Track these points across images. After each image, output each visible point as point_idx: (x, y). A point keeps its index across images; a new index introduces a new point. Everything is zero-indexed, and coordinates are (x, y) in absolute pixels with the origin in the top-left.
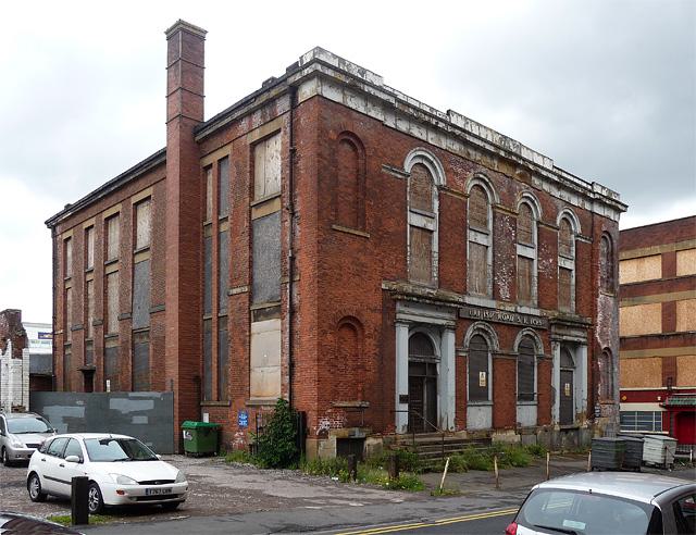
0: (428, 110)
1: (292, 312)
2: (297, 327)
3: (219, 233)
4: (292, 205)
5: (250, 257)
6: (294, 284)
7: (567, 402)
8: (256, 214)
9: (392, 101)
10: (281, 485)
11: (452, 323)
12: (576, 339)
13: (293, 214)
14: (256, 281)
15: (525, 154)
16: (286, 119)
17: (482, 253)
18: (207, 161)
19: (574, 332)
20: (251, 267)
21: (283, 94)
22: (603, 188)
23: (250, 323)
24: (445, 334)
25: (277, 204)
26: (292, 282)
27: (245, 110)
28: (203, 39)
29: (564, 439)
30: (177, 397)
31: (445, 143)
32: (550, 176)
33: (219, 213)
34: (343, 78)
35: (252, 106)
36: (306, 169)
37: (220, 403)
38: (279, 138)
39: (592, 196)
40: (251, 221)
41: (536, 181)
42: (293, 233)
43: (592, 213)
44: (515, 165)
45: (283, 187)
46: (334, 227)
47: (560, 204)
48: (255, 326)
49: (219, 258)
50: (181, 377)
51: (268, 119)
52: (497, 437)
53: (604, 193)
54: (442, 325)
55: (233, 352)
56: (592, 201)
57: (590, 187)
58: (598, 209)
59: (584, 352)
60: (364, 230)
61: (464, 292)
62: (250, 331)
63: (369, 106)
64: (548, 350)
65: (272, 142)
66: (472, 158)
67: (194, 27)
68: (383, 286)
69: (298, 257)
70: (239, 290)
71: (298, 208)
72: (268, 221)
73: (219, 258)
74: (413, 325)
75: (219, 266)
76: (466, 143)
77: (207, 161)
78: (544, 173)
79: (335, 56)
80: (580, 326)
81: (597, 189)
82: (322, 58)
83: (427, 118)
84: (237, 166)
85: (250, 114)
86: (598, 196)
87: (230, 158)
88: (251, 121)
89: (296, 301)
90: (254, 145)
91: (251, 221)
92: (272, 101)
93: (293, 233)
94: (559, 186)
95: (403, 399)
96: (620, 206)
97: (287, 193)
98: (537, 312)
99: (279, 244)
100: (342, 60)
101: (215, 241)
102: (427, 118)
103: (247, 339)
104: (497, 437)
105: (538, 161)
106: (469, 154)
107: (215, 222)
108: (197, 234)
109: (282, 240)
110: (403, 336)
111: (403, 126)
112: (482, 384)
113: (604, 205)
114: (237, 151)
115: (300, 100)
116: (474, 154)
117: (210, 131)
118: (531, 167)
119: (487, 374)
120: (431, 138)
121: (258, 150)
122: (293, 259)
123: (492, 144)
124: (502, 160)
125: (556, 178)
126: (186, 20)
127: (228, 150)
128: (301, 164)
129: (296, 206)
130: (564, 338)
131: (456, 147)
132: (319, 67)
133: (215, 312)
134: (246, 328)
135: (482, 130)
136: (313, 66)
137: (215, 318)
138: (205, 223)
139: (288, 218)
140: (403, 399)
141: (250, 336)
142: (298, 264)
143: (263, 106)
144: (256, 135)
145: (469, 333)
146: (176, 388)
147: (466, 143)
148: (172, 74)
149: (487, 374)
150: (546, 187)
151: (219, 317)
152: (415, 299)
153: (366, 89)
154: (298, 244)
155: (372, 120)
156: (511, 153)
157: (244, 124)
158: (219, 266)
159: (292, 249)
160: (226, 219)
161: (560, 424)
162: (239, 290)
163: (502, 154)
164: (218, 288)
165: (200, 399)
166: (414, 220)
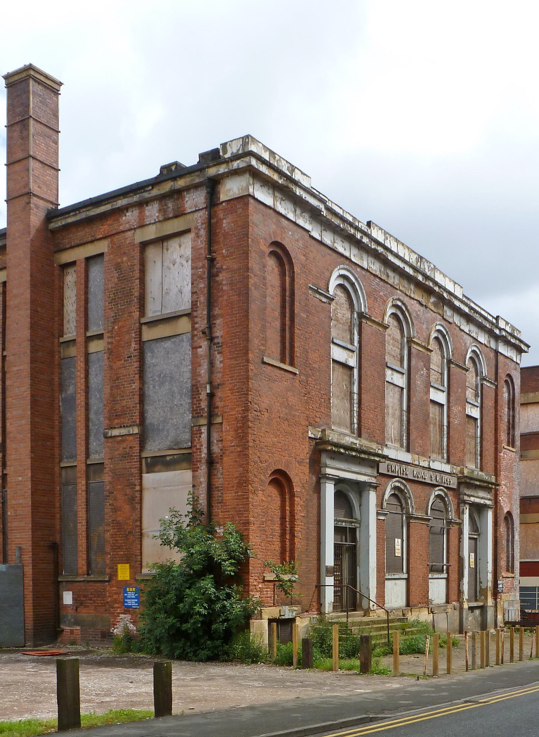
0: (350, 219)
1: (211, 462)
2: (219, 480)
3: (87, 355)
4: (210, 326)
5: (141, 389)
6: (214, 429)
7: (475, 572)
8: (148, 334)
9: (322, 207)
10: (487, 671)
11: (374, 480)
12: (482, 501)
13: (211, 339)
14: (148, 422)
15: (439, 278)
16: (201, 217)
17: (397, 396)
18: (66, 257)
19: (481, 494)
20: (142, 401)
21: (196, 187)
22: (507, 323)
23: (141, 473)
24: (364, 495)
25: (184, 325)
26: (210, 425)
27: (136, 198)
28: (56, 93)
29: (470, 619)
30: (29, 570)
31: (366, 262)
32: (463, 307)
33: (86, 328)
34: (275, 177)
35: (146, 195)
36: (231, 284)
37: (92, 577)
38: (187, 241)
39: (497, 332)
40: (141, 344)
41: (448, 313)
42: (211, 364)
43: (497, 352)
44: (429, 292)
45: (194, 304)
46: (266, 359)
47: (469, 340)
48: (149, 478)
49: (87, 386)
50: (35, 545)
51: (171, 215)
52: (412, 617)
53: (508, 329)
54: (365, 483)
55: (115, 510)
56: (497, 338)
57: (494, 321)
58: (502, 349)
59: (490, 514)
60: (292, 364)
61: (383, 444)
62: (141, 485)
63: (298, 211)
64: (459, 513)
65: (173, 244)
66: (391, 281)
67: (46, 77)
68: (310, 435)
69: (219, 394)
70: (123, 431)
71: (218, 333)
72: (168, 344)
73: (87, 386)
74: (339, 481)
75: (87, 398)
76: (386, 263)
77: (66, 257)
78: (457, 303)
79: (266, 148)
80: (486, 486)
81: (502, 325)
82: (253, 148)
83: (352, 231)
84: (118, 267)
85: (142, 204)
86: (504, 333)
87: (106, 258)
88: (141, 213)
89: (216, 449)
90: (144, 245)
91: (141, 344)
92: (177, 194)
93: (211, 364)
94: (469, 319)
95: (330, 571)
96: (523, 346)
97: (202, 312)
98: (447, 468)
99: (188, 375)
100: (272, 153)
101: (81, 365)
102: (352, 231)
103: (138, 495)
104: (412, 617)
105: (450, 287)
106: (388, 276)
107: (81, 340)
108: (52, 353)
109: (194, 373)
110: (329, 490)
111: (328, 238)
112: (398, 554)
113: (508, 343)
114: (117, 249)
115: (223, 197)
116: (394, 279)
117: (78, 218)
118: (445, 295)
119: (402, 541)
120: (353, 254)
121: (152, 253)
122: (211, 396)
123: (411, 266)
124: (419, 285)
125: (467, 310)
126: (38, 65)
127: (102, 247)
128: (222, 277)
129: (215, 330)
130: (472, 499)
131: (376, 267)
132: (254, 162)
133: (81, 456)
134: (137, 482)
135: (400, 247)
136: (247, 159)
137: (83, 467)
138: (62, 340)
139: (205, 344)
140: (330, 571)
141: (141, 491)
142: (219, 404)
143: (162, 198)
144: (151, 233)
145: (388, 492)
146: (28, 557)
147: (386, 263)
148: (16, 134)
149: (402, 541)
150: (457, 319)
151: (88, 466)
152: (342, 450)
153: (298, 192)
154: (218, 378)
155: (300, 230)
156: (427, 277)
157: (131, 217)
158: (87, 398)
159: (211, 383)
160: (100, 337)
161: (469, 601)
162: (123, 431)
163: (420, 278)
164: (87, 427)
165: (57, 572)
166: (337, 354)
